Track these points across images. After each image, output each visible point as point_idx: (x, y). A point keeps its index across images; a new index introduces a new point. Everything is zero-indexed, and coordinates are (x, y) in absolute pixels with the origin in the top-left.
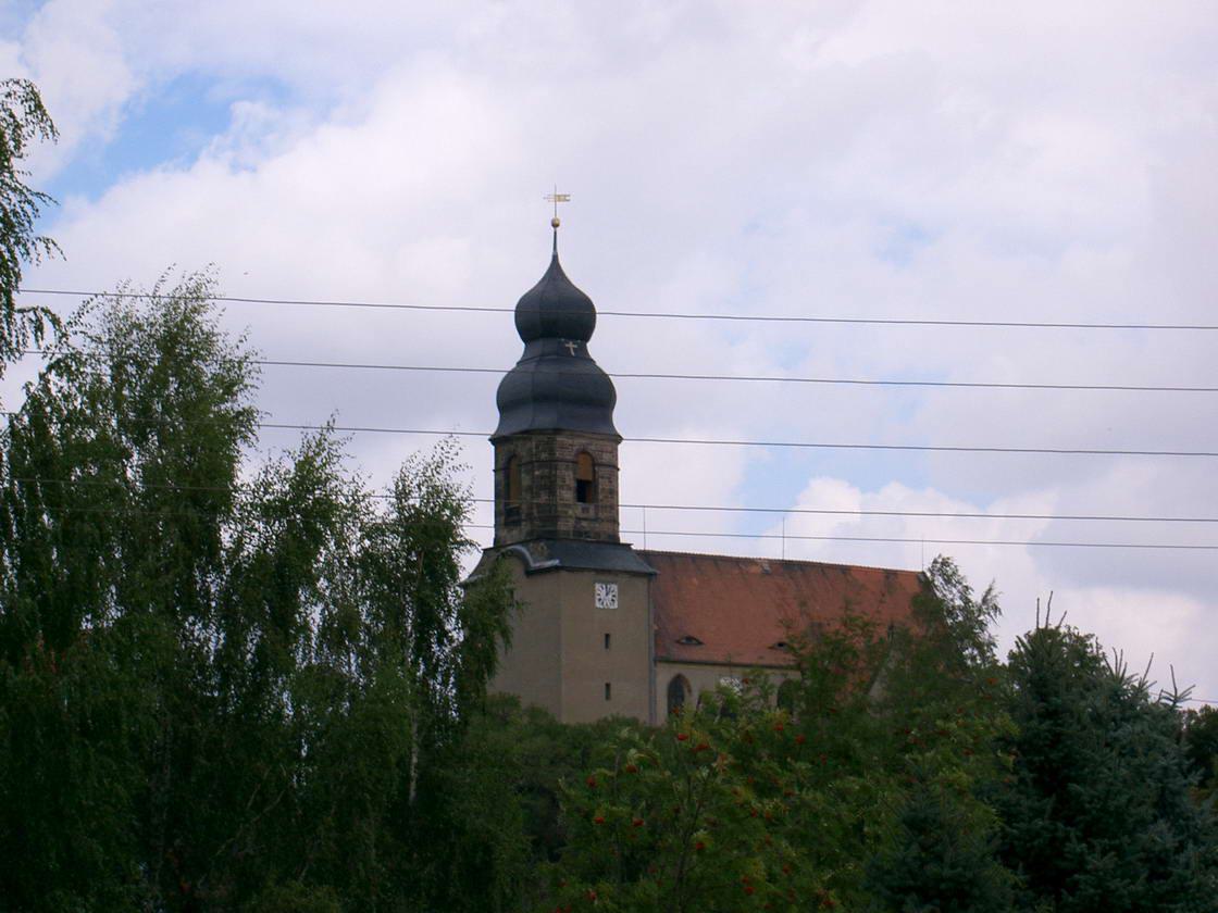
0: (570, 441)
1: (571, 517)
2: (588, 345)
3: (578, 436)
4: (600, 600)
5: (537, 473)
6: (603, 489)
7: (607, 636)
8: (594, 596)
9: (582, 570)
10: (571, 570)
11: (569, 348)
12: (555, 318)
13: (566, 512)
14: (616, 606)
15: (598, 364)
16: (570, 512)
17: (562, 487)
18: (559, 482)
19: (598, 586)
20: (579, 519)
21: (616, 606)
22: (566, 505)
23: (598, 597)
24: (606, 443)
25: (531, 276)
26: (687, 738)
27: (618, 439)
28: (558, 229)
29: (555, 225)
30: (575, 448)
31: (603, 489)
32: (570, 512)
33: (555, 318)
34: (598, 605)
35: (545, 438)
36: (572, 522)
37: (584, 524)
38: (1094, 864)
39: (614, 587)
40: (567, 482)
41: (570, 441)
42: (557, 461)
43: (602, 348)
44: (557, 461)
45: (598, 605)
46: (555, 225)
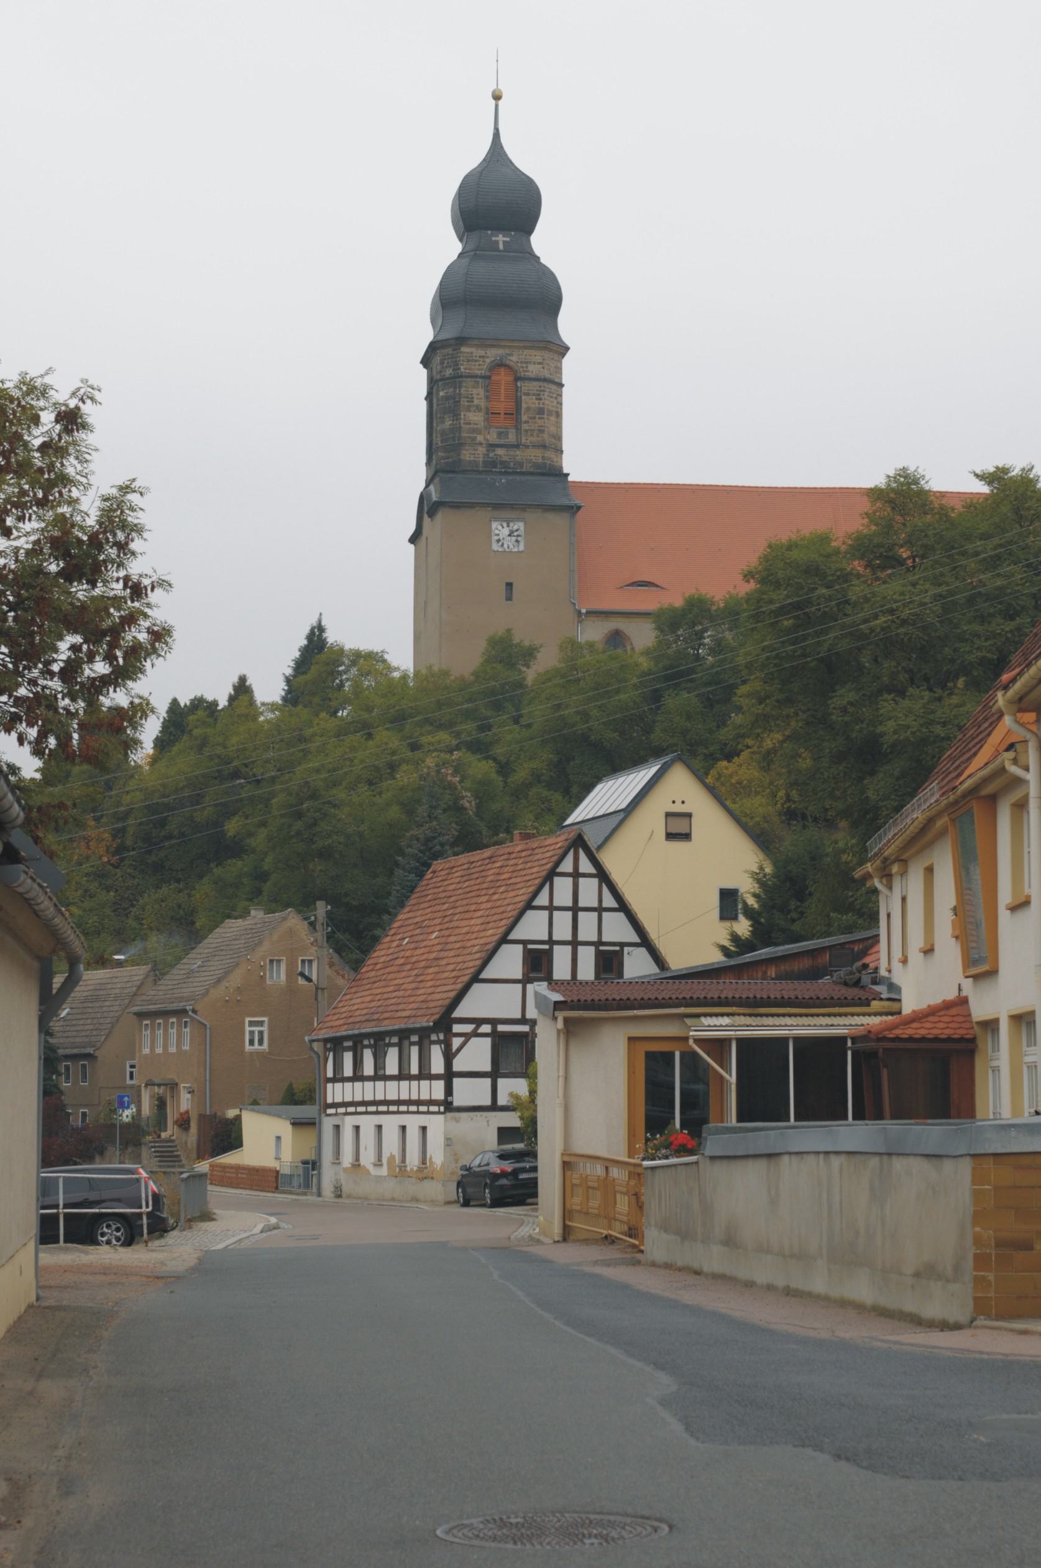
0: (482, 353)
1: (481, 444)
2: (534, 238)
3: (493, 346)
4: (498, 541)
5: (441, 394)
6: (528, 409)
7: (509, 585)
8: (490, 537)
9: (472, 506)
10: (456, 506)
11: (497, 242)
12: (497, 208)
13: (474, 439)
14: (522, 547)
15: (543, 261)
16: (480, 438)
17: (468, 409)
18: (464, 402)
19: (495, 525)
20: (492, 446)
21: (522, 547)
22: (475, 431)
23: (496, 538)
24: (533, 352)
25: (472, 155)
26: (105, 770)
27: (564, 350)
28: (500, 102)
29: (497, 97)
30: (488, 360)
31: (528, 409)
32: (480, 438)
33: (497, 208)
34: (495, 547)
35: (449, 350)
36: (482, 450)
37: (500, 452)
38: (265, 974)
39: (520, 525)
40: (476, 402)
41: (482, 353)
42: (461, 376)
43: (547, 242)
44: (461, 376)
45: (495, 547)
46: (497, 97)
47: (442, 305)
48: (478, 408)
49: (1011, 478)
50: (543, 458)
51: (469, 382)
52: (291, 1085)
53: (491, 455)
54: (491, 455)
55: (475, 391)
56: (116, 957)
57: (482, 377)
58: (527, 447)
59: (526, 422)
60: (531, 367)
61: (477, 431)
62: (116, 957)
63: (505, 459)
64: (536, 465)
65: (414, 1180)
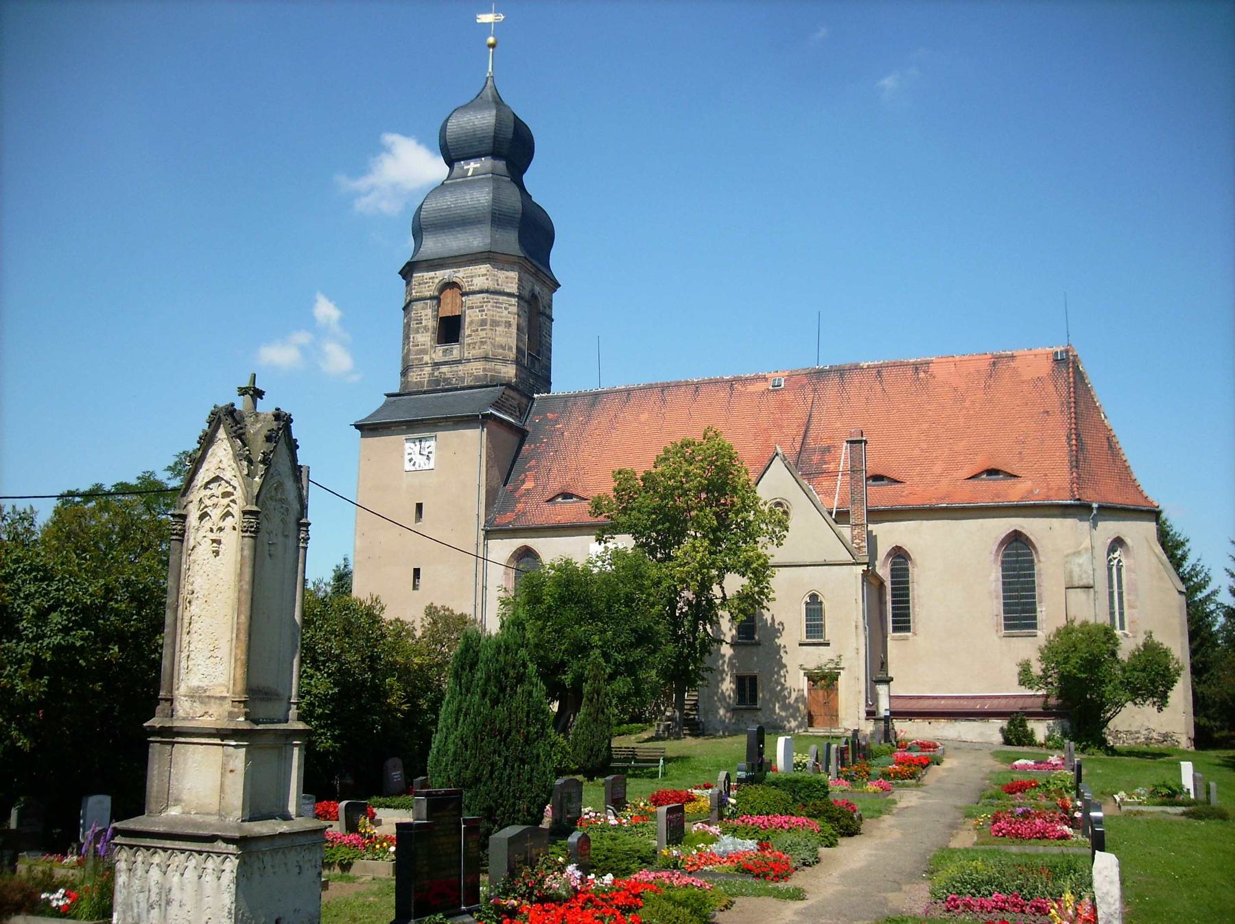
6: (471, 323)
14: (432, 465)
20: (437, 365)
30: (437, 281)
32: (426, 358)
36: (428, 370)
37: (444, 369)
47: (493, 214)
48: (426, 329)
49: (47, 531)
50: (484, 370)
51: (419, 304)
52: (1160, 710)
53: (436, 374)
54: (436, 374)
55: (424, 313)
56: (14, 813)
57: (431, 298)
58: (469, 361)
59: (470, 336)
60: (475, 281)
61: (424, 352)
62: (14, 813)
63: (449, 375)
64: (477, 378)
65: (1032, 841)
